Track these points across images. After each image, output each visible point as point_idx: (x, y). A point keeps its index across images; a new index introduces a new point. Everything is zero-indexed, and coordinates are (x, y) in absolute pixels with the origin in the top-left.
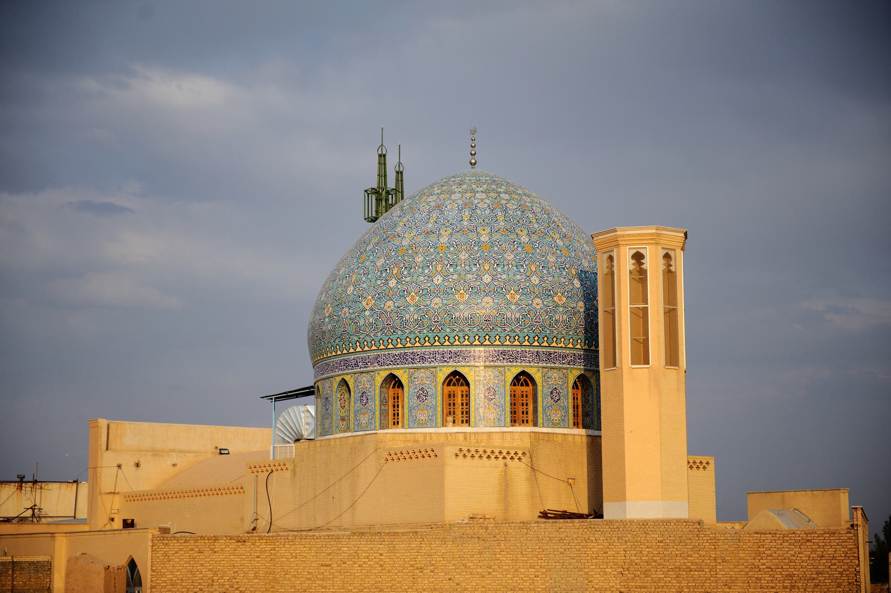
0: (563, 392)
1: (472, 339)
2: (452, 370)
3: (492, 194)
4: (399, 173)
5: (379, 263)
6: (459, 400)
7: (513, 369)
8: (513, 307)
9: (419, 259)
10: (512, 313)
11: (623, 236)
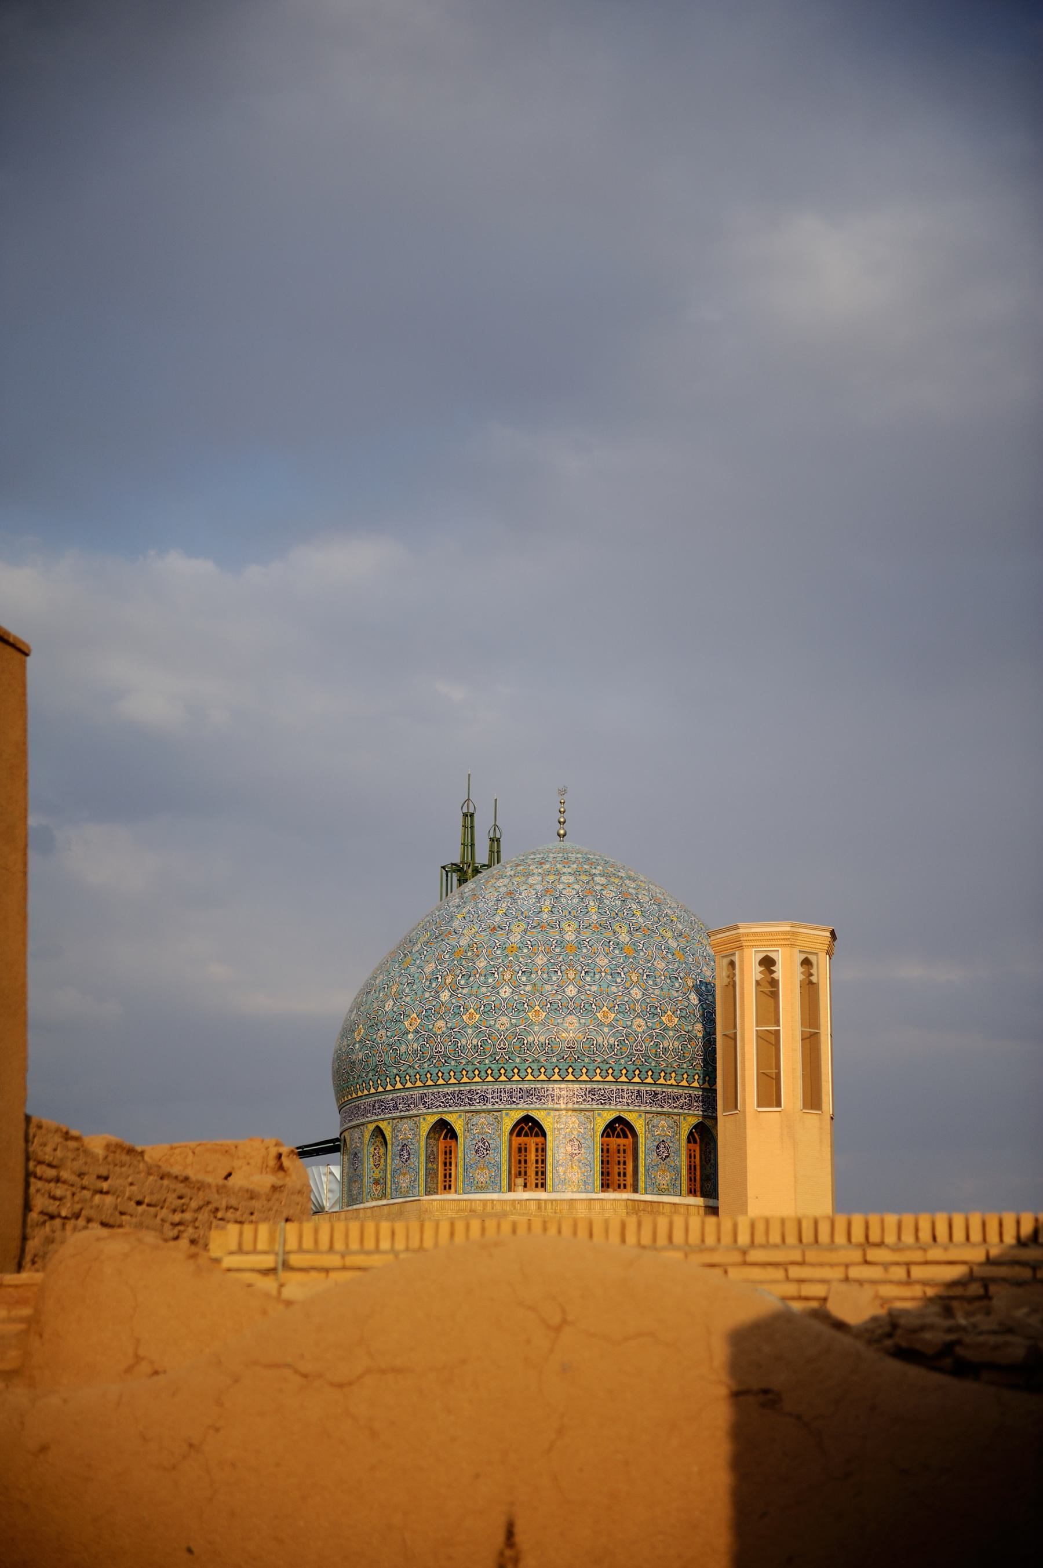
0: (674, 1147)
1: (550, 1072)
2: (522, 1114)
3: (584, 878)
4: (495, 841)
5: (429, 969)
6: (532, 1157)
7: (605, 1114)
8: (606, 1030)
9: (481, 964)
10: (605, 1038)
11: (748, 935)
